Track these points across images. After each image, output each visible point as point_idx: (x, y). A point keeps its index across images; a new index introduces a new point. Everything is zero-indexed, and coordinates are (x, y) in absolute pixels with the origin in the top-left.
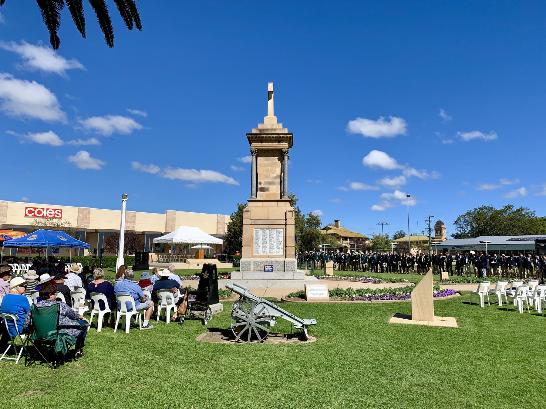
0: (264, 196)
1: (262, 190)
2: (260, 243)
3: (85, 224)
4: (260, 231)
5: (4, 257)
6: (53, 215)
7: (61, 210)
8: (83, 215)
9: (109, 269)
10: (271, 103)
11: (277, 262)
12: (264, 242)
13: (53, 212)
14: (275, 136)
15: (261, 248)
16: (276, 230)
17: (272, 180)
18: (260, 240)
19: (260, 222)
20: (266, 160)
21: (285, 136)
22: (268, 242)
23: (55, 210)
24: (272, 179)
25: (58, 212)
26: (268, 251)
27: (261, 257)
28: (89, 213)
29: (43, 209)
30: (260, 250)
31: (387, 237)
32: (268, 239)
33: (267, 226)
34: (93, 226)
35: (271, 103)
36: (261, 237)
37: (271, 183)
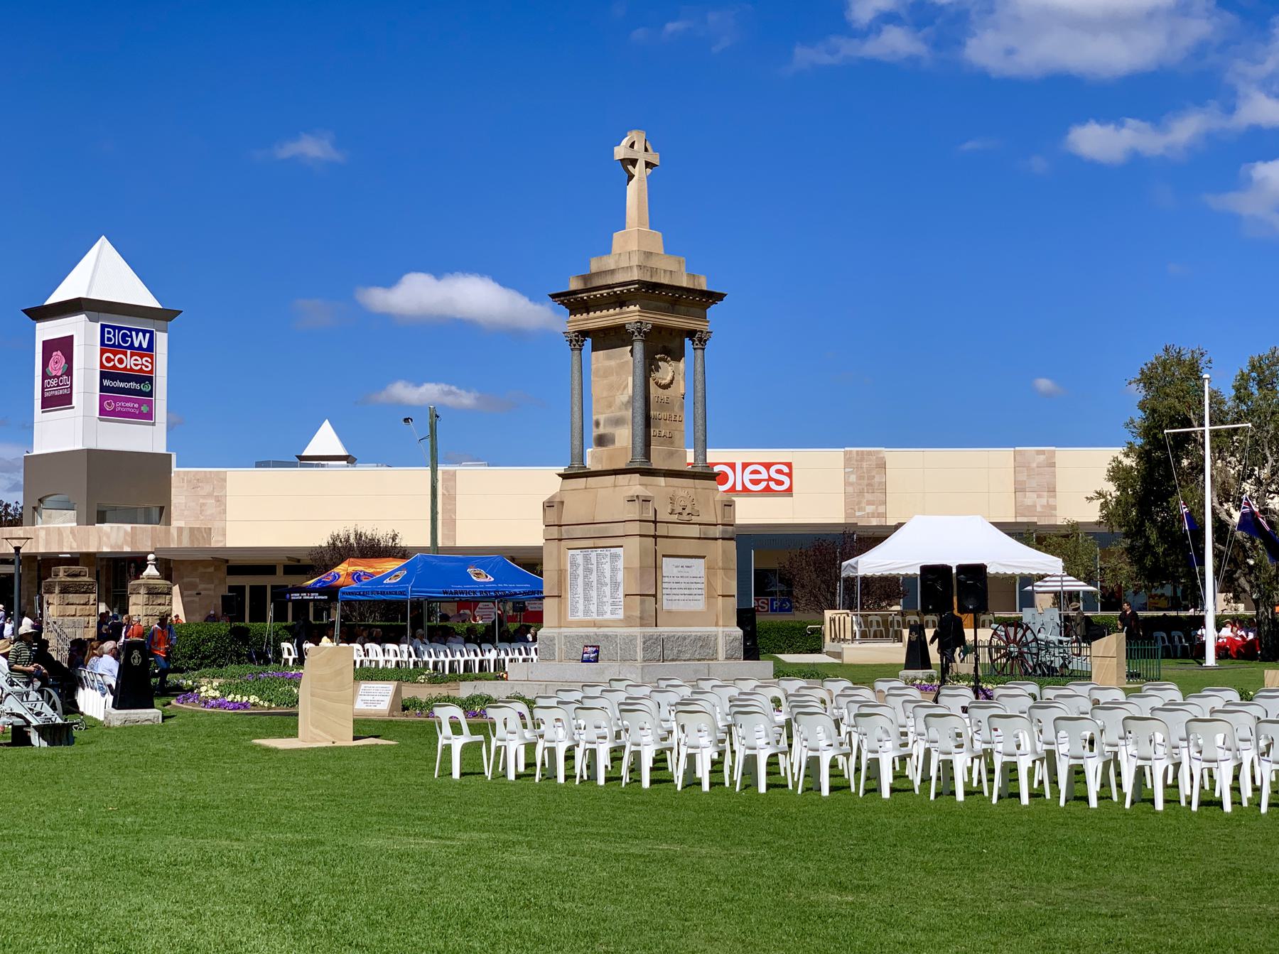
1: (602, 441)
2: (580, 590)
3: (870, 509)
6: (763, 484)
7: (789, 465)
8: (860, 478)
10: (635, 193)
11: (607, 637)
12: (587, 585)
13: (764, 475)
14: (604, 292)
15: (581, 601)
16: (607, 552)
17: (619, 414)
18: (580, 581)
19: (578, 531)
20: (609, 358)
22: (595, 584)
23: (768, 466)
24: (620, 409)
25: (779, 472)
26: (594, 608)
27: (581, 624)
28: (882, 466)
29: (732, 466)
30: (581, 607)
32: (594, 577)
35: (635, 193)
36: (580, 571)
37: (618, 422)
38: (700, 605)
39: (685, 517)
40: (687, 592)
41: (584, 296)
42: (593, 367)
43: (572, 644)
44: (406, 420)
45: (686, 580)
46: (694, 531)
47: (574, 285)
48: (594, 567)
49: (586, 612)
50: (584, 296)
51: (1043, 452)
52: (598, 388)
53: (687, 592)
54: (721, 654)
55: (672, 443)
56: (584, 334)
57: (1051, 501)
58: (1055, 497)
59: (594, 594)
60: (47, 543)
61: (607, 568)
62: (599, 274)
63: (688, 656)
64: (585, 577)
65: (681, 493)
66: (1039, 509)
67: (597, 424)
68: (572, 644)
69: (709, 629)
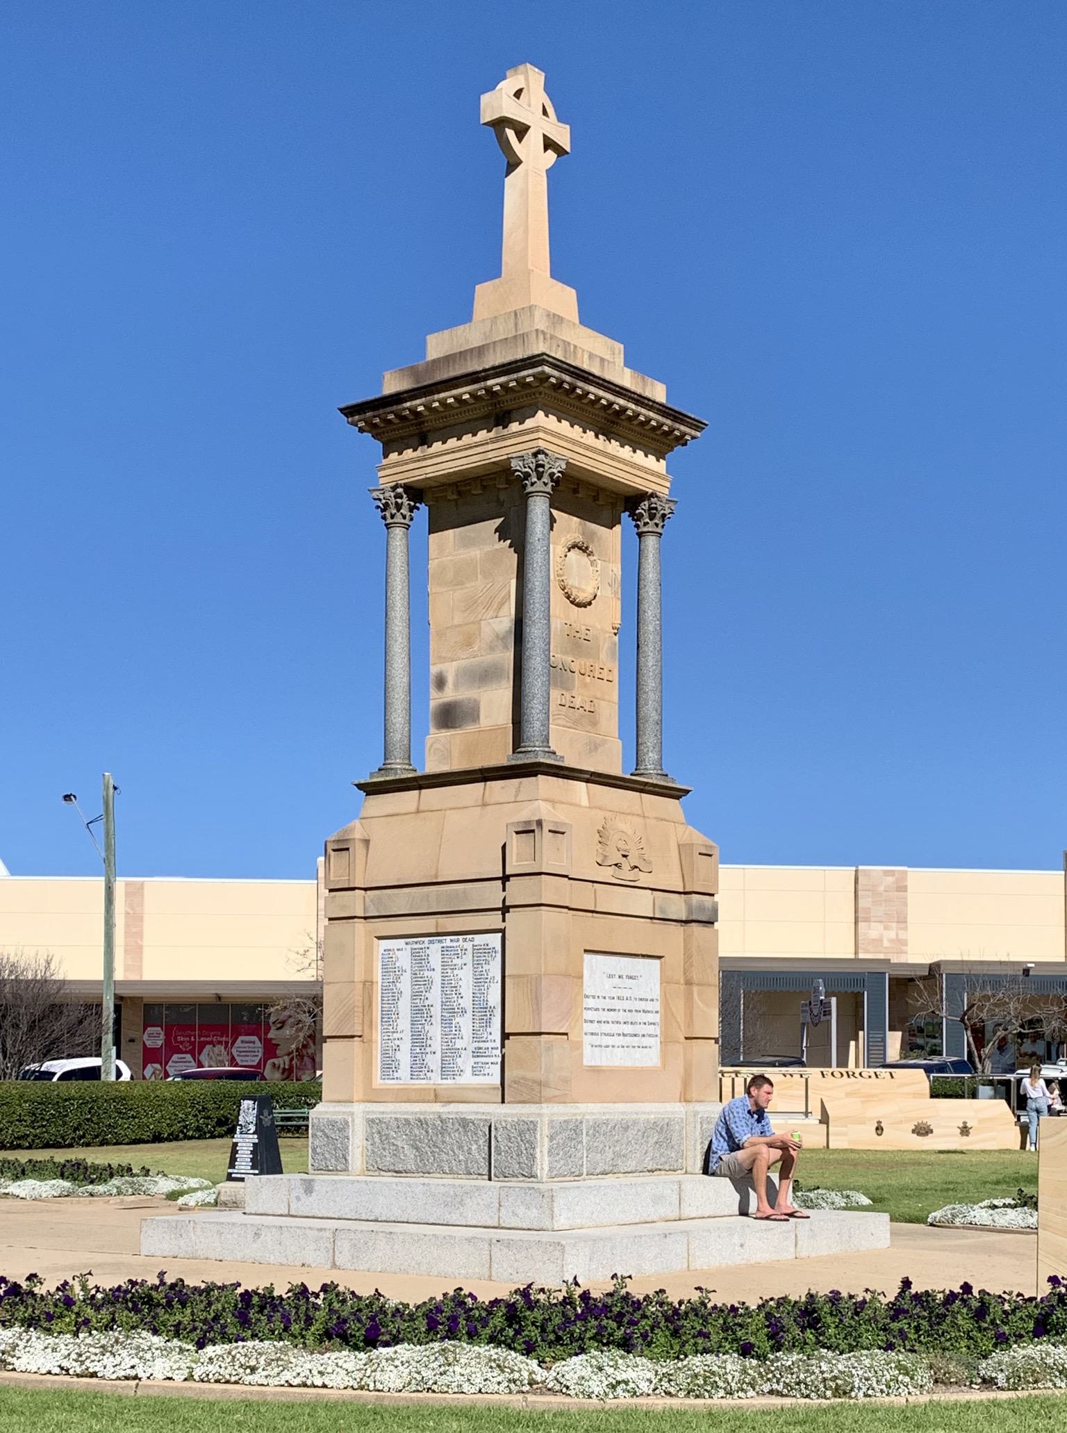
0: (455, 753)
1: (449, 716)
2: (404, 1023)
4: (402, 952)
5: (532, 1127)
9: (986, 1203)
10: (526, 198)
12: (420, 1013)
14: (464, 392)
15: (406, 1046)
17: (489, 658)
18: (404, 1005)
19: (401, 901)
20: (467, 543)
21: (510, 380)
22: (436, 1011)
24: (492, 648)
26: (434, 1062)
30: (404, 1057)
31: (48, 963)
33: (428, 924)
34: (919, 950)
35: (526, 198)
36: (405, 985)
37: (485, 676)
38: (650, 1057)
39: (626, 874)
40: (628, 1029)
41: (419, 404)
42: (432, 565)
43: (385, 1138)
44: (67, 798)
45: (627, 1005)
46: (643, 903)
47: (392, 385)
48: (437, 977)
49: (419, 1067)
50: (419, 404)
51: (892, 873)
52: (444, 606)
53: (628, 1029)
54: (357, 1158)
55: (594, 724)
56: (415, 492)
57: (902, 935)
58: (906, 929)
59: (435, 1031)
60: (127, 969)
61: (465, 978)
62: (448, 359)
63: (632, 1164)
64: (415, 995)
65: (624, 825)
66: (886, 944)
67: (441, 683)
68: (385, 1138)
69: (669, 1107)
